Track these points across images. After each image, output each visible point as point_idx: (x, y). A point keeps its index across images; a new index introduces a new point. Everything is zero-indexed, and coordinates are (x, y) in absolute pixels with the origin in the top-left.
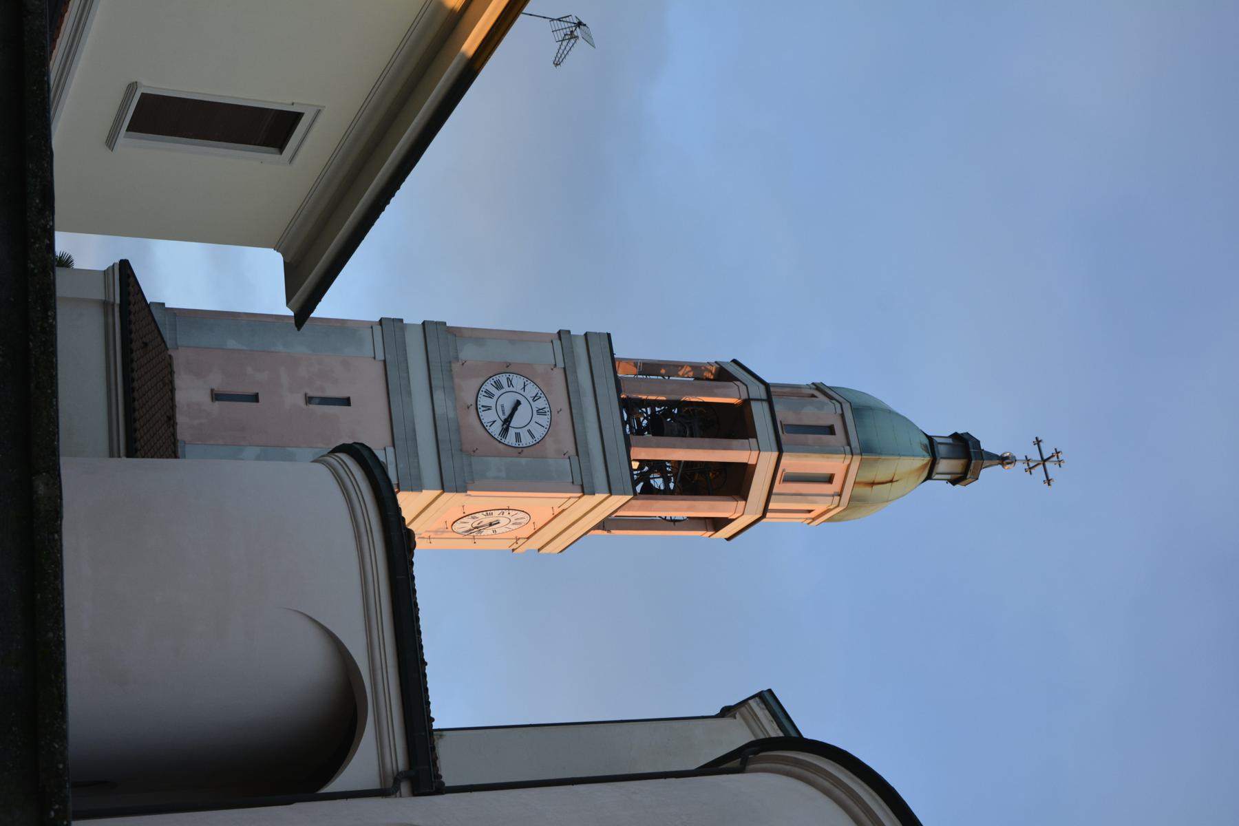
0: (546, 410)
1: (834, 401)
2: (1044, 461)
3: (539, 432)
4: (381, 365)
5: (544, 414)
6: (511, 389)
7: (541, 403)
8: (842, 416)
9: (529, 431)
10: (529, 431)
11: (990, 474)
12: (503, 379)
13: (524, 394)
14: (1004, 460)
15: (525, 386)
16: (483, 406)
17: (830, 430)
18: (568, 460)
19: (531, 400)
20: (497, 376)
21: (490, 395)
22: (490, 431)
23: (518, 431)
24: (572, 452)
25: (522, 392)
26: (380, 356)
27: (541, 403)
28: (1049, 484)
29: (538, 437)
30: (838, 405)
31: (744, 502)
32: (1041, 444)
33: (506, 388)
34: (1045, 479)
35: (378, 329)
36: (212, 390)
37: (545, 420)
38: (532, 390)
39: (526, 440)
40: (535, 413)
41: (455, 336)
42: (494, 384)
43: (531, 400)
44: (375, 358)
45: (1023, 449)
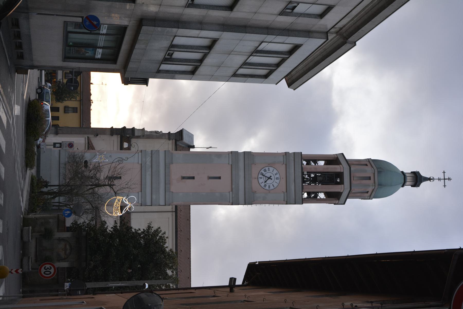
0: (279, 178)
1: (372, 168)
2: (445, 179)
3: (276, 185)
4: (230, 166)
5: (278, 179)
6: (269, 172)
7: (278, 176)
8: (374, 173)
9: (273, 185)
10: (273, 185)
11: (423, 184)
12: (267, 168)
13: (275, 176)
14: (429, 179)
15: (273, 170)
16: (260, 177)
17: (369, 178)
18: (283, 194)
19: (274, 175)
20: (265, 168)
21: (269, 186)
22: (259, 180)
23: (269, 185)
24: (285, 191)
25: (272, 172)
26: (230, 163)
27: (278, 176)
28: (445, 187)
29: (275, 186)
30: (373, 170)
31: (338, 201)
32: (445, 173)
33: (267, 171)
34: (444, 185)
35: (230, 155)
36: (147, 86)
37: (278, 181)
38: (275, 172)
39: (272, 187)
40: (275, 179)
41: (213, 76)
42: (264, 170)
43: (274, 175)
44: (229, 164)
45: (437, 174)
